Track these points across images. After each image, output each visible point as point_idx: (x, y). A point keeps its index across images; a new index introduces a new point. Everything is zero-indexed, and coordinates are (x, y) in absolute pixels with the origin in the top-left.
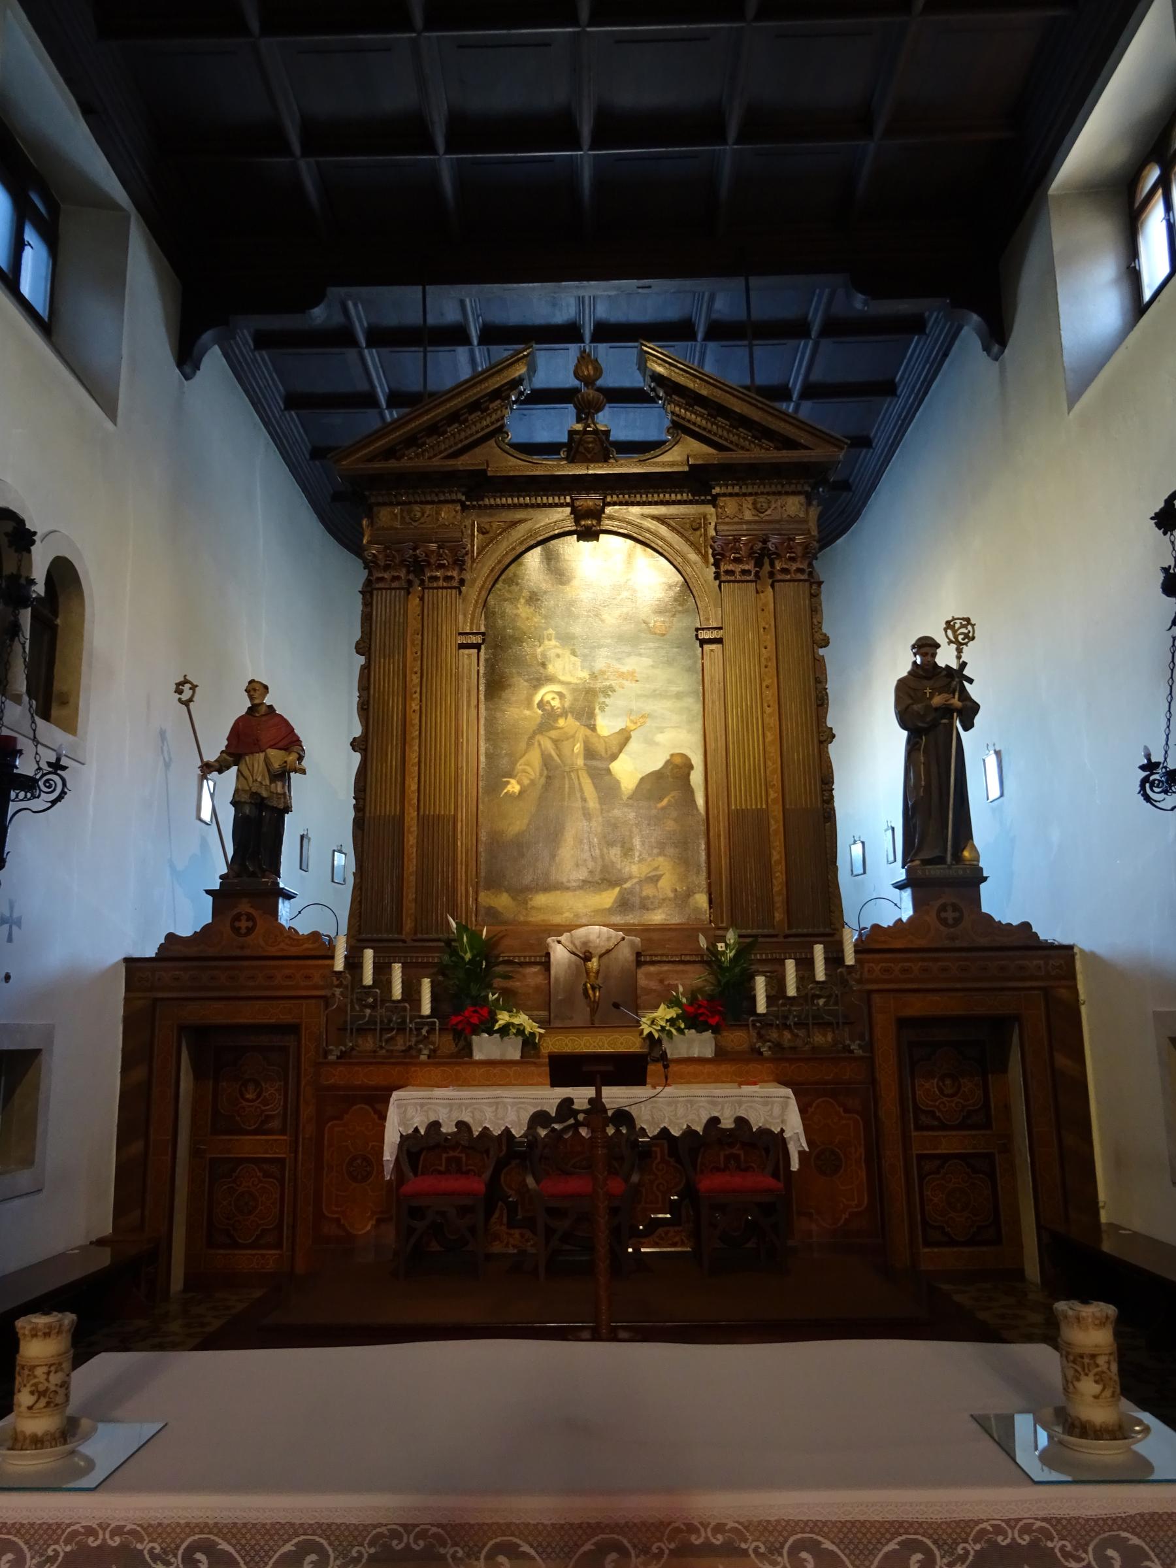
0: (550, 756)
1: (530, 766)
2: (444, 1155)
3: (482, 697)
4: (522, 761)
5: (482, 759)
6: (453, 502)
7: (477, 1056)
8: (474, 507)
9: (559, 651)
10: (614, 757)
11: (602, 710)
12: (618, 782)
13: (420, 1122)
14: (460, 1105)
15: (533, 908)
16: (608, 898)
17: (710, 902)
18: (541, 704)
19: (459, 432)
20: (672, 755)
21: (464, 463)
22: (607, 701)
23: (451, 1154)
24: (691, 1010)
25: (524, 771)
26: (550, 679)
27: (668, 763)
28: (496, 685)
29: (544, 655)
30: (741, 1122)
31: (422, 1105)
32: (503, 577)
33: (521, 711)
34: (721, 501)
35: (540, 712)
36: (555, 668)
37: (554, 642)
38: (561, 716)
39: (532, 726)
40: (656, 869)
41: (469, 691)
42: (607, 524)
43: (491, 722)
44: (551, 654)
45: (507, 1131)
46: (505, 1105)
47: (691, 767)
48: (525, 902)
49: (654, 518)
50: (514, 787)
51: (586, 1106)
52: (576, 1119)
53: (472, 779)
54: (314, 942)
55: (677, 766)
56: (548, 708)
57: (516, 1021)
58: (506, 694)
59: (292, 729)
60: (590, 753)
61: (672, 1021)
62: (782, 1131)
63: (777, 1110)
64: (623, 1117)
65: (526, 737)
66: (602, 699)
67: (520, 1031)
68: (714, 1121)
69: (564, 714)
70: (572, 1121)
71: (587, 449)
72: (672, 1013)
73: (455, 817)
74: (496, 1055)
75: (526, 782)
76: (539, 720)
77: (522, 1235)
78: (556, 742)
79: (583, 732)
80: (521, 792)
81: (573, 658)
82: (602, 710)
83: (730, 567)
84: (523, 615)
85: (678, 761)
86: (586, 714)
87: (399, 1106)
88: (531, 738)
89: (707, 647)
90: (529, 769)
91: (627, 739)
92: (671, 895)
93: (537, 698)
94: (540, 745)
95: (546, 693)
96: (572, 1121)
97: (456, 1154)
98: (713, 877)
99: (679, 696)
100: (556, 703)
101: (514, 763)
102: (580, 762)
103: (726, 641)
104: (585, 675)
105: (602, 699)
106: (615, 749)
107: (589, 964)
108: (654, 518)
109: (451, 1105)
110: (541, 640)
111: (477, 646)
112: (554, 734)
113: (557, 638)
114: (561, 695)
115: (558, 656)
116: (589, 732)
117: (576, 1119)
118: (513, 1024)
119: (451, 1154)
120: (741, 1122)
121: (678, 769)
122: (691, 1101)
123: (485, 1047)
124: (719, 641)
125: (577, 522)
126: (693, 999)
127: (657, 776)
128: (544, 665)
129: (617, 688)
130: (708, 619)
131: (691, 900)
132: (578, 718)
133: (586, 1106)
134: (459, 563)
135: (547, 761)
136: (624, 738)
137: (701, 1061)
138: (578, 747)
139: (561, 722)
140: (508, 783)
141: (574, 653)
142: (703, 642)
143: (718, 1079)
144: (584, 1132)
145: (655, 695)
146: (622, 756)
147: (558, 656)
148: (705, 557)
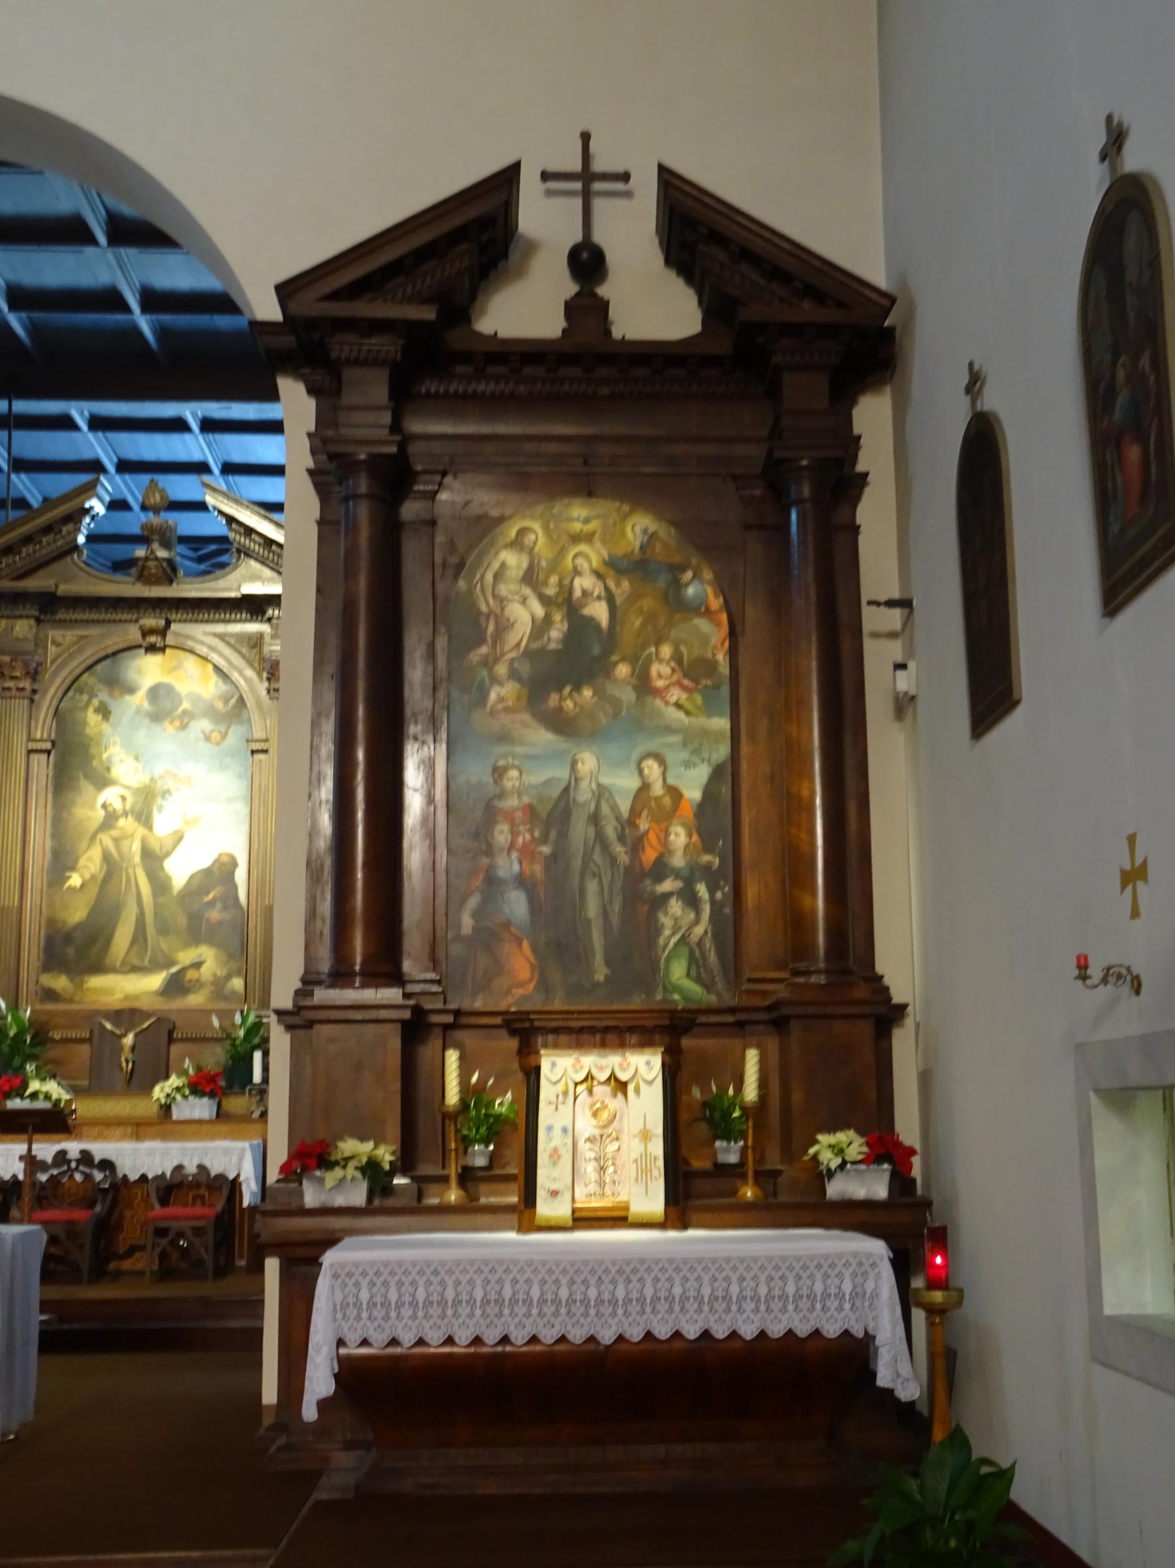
0: (111, 854)
1: (90, 863)
4: (86, 856)
6: (27, 617)
8: (49, 621)
10: (168, 854)
15: (88, 989)
16: (156, 981)
18: (104, 806)
19: (34, 552)
21: (34, 584)
25: (86, 867)
29: (109, 759)
30: (202, 1168)
32: (75, 685)
33: (92, 806)
36: (116, 772)
38: (122, 816)
40: (200, 956)
42: (170, 639)
48: (81, 984)
49: (216, 635)
50: (75, 880)
59: (321, 523)
61: (178, 1089)
62: (238, 1176)
63: (235, 1159)
64: (107, 1165)
65: (89, 836)
68: (179, 1168)
69: (125, 814)
75: (87, 876)
78: (116, 841)
79: (141, 831)
80: (82, 886)
81: (135, 763)
82: (160, 809)
85: (225, 859)
86: (144, 817)
91: (180, 839)
94: (101, 841)
95: (110, 796)
96: (65, 1168)
100: (118, 805)
101: (76, 861)
102: (137, 859)
103: (271, 751)
104: (144, 779)
105: (159, 801)
108: (216, 635)
111: (49, 752)
112: (114, 833)
114: (124, 798)
115: (122, 761)
120: (202, 1168)
121: (223, 871)
122: (151, 1152)
124: (265, 751)
127: (207, 872)
134: (34, 675)
135: (106, 857)
136: (179, 838)
137: (200, 1122)
138: (136, 847)
139: (122, 822)
140: (69, 877)
141: (137, 758)
143: (213, 1137)
148: (259, 674)
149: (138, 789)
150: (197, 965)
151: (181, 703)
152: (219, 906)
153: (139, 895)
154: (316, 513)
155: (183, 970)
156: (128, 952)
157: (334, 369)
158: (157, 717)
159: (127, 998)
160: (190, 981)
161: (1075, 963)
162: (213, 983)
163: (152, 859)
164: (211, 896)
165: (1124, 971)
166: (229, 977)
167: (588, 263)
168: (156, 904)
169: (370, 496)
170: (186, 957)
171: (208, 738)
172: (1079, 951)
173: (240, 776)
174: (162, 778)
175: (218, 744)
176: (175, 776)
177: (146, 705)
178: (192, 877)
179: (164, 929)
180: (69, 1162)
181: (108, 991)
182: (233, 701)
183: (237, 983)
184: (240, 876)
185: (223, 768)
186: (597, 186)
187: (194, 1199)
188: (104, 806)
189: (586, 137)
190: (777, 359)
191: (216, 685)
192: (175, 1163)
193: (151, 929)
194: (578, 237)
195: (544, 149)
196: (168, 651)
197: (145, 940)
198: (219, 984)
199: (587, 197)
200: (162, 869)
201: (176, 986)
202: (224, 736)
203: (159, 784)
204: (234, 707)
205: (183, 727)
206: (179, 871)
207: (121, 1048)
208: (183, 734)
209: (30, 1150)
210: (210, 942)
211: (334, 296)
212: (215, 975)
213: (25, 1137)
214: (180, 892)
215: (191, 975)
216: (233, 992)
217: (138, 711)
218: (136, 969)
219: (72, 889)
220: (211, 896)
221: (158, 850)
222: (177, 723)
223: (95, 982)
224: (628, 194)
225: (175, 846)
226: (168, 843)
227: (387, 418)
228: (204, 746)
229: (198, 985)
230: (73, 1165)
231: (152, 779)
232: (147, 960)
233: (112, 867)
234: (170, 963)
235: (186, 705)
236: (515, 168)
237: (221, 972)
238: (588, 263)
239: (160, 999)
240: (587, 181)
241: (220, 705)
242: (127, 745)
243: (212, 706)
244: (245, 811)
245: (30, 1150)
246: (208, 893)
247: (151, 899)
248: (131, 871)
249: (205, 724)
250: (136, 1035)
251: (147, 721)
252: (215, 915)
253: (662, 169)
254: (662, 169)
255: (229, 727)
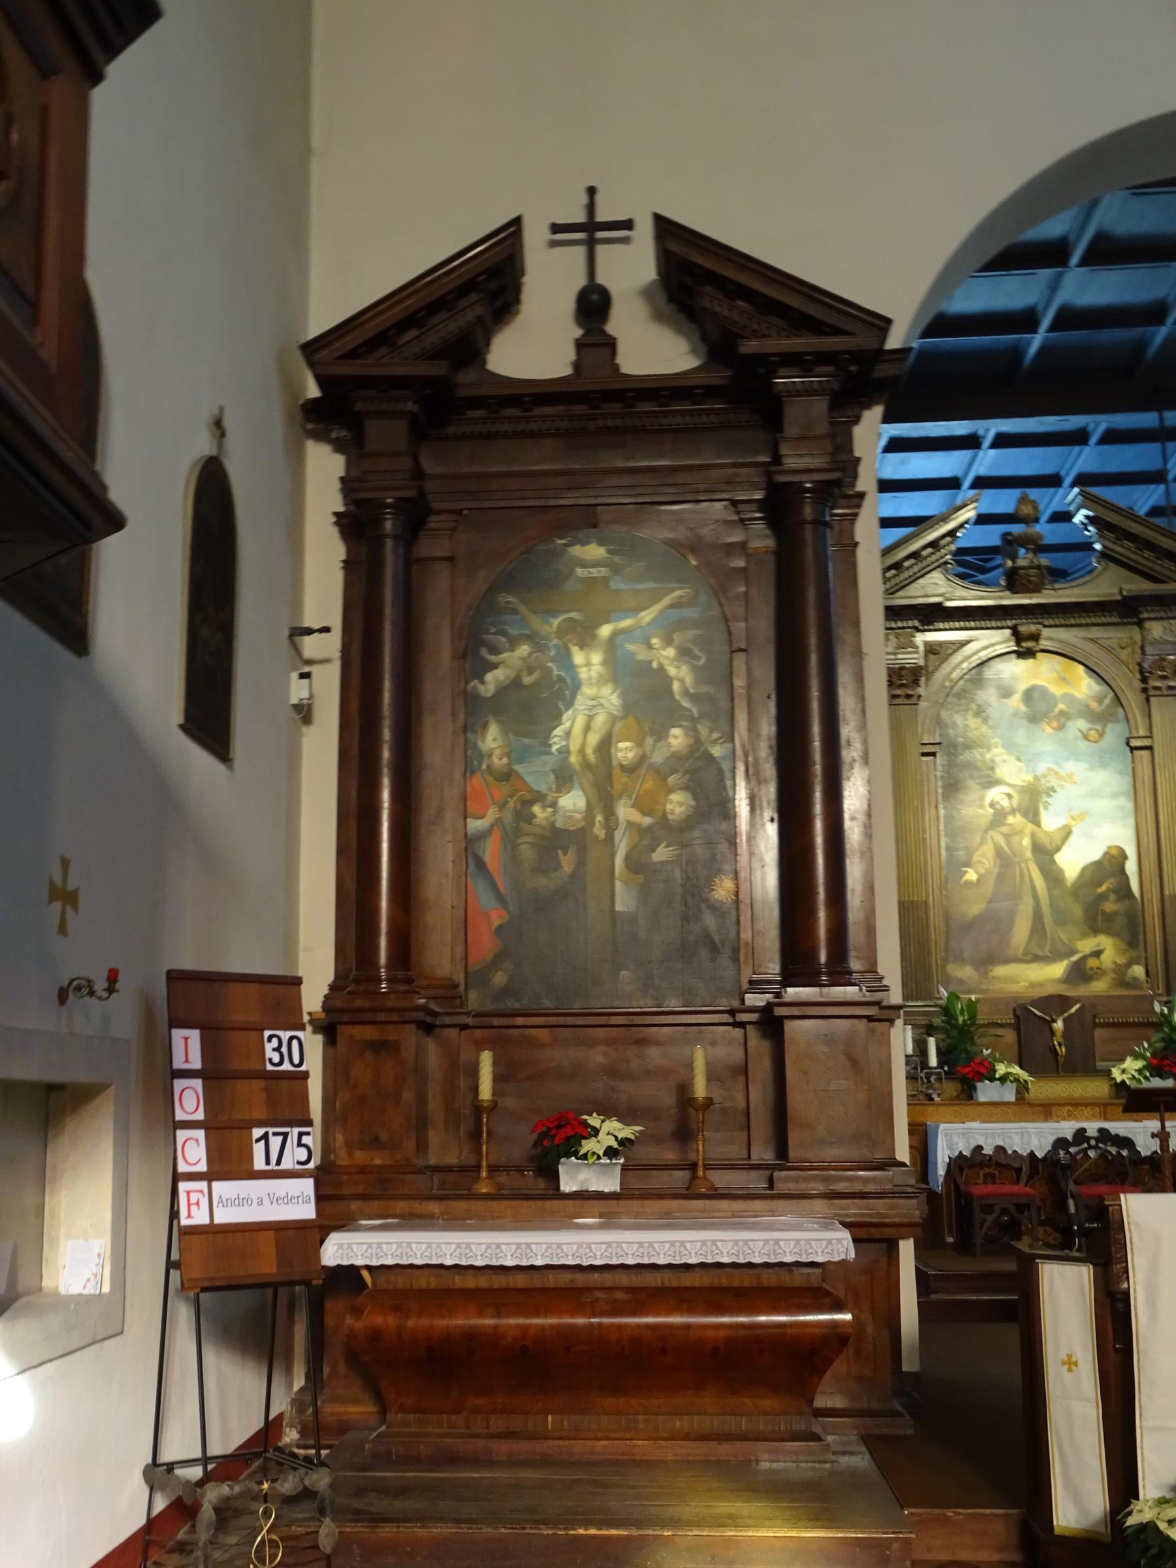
2: (981, 1172)
3: (940, 797)
4: (977, 853)
5: (943, 852)
7: (982, 1098)
9: (1005, 757)
10: (1058, 849)
11: (1046, 808)
12: (1061, 871)
13: (964, 1147)
14: (993, 1134)
16: (1058, 970)
17: (1147, 973)
18: (992, 805)
20: (1109, 848)
22: (1050, 800)
23: (987, 1170)
24: (1155, 1062)
25: (980, 862)
26: (997, 782)
27: (1106, 854)
28: (953, 787)
29: (992, 760)
31: (964, 1134)
34: (1148, 624)
35: (991, 811)
36: (1002, 772)
37: (999, 750)
38: (1009, 814)
39: (985, 822)
40: (1099, 945)
41: (25, 398)
42: (1044, 643)
43: (949, 818)
44: (998, 760)
45: (1032, 1154)
46: (1028, 1133)
47: (1125, 857)
48: (987, 973)
50: (971, 875)
51: (1096, 1134)
52: (1089, 1143)
53: (936, 869)
54: (776, 997)
55: (1113, 857)
56: (998, 807)
57: (1013, 1071)
58: (960, 796)
60: (1037, 848)
61: (1140, 1071)
66: (1045, 798)
67: (1017, 1080)
69: (1013, 811)
70: (1086, 1145)
71: (1030, 582)
72: (1140, 1064)
73: (926, 902)
74: (996, 1098)
76: (991, 817)
77: (1045, 1231)
78: (1007, 837)
79: (1030, 827)
80: (978, 880)
82: (1046, 808)
83: (1158, 684)
84: (973, 726)
85: (1115, 852)
86: (1032, 815)
87: (946, 1135)
88: (986, 831)
89: (1136, 752)
90: (985, 861)
92: (1113, 966)
93: (988, 800)
95: (995, 794)
96: (1086, 1145)
97: (991, 1171)
98: (1149, 951)
99: (1114, 795)
100: (1005, 803)
102: (1029, 854)
104: (1029, 778)
105: (1045, 798)
106: (1059, 843)
107: (1055, 1025)
109: (987, 1134)
110: (989, 749)
112: (1004, 829)
113: (1003, 747)
114: (1009, 796)
115: (1005, 761)
116: (1034, 828)
117: (1089, 1143)
118: (1010, 1074)
119: (987, 1170)
121: (1113, 862)
123: (986, 1092)
125: (1018, 643)
126: (1154, 1055)
127: (1098, 865)
128: (992, 769)
129: (1058, 789)
130: (1137, 729)
131: (1130, 971)
132: (1025, 815)
133: (1096, 1134)
135: (999, 852)
136: (1067, 833)
137: (1008, 1104)
138: (1026, 842)
139: (1011, 820)
140: (966, 872)
141: (1018, 759)
142: (1132, 749)
144: (1092, 1153)
145: (1095, 794)
146: (1064, 848)
147: (1005, 761)
149: (1023, 787)
150: (1097, 954)
151: (1056, 705)
152: (1112, 897)
153: (1033, 887)
154: (342, 555)
155: (1084, 959)
156: (1028, 943)
157: (356, 424)
158: (1034, 719)
159: (1033, 985)
160: (1091, 969)
161: (106, 975)
162: (1114, 971)
163: (1045, 853)
164: (1104, 888)
165: (84, 983)
166: (1129, 965)
167: (593, 305)
168: (1051, 896)
169: (395, 537)
170: (1086, 946)
171: (1086, 737)
172: (112, 966)
173: (1121, 773)
174: (1045, 776)
175: (1096, 742)
176: (1057, 773)
177: (1023, 708)
178: (1084, 869)
179: (1061, 920)
180: (1088, 1139)
181: (1013, 980)
182: (1107, 701)
183: (1138, 971)
184: (1131, 867)
185: (1104, 765)
186: (600, 235)
187: (985, 1175)
188: (992, 805)
189: (592, 191)
190: (359, 407)
191: (1089, 687)
192: (973, 1144)
193: (1048, 920)
194: (581, 281)
195: (545, 205)
196: (1039, 655)
197: (1044, 931)
198: (1120, 972)
199: (591, 244)
200: (1054, 862)
201: (1080, 973)
202: (1101, 735)
203: (1043, 781)
204: (1109, 706)
205: (1061, 727)
206: (1073, 861)
207: (1052, 1033)
208: (1061, 734)
209: (1163, 1127)
210: (1109, 932)
211: (352, 355)
212: (1115, 963)
213: (1158, 1115)
214: (1074, 884)
215: (1092, 963)
216: (1136, 979)
217: (1015, 714)
218: (1037, 959)
219: (969, 884)
220: (1104, 888)
221: (1048, 846)
222: (1055, 724)
223: (1000, 971)
224: (626, 241)
225: (1064, 839)
226: (1057, 840)
227: (406, 463)
228: (1083, 744)
229: (1099, 973)
230: (1093, 1142)
231: (1036, 778)
232: (1047, 949)
233: (1005, 860)
234: (1074, 952)
235: (1061, 706)
236: (513, 229)
237: (1121, 960)
238: (593, 305)
239: (1065, 986)
240: (591, 231)
241: (1094, 705)
242: (1009, 746)
243: (1087, 706)
244: (1130, 805)
245: (1163, 1127)
246: (1100, 885)
247: (1045, 890)
248: (1023, 865)
249: (1082, 724)
250: (1065, 1021)
251: (1025, 722)
252: (1110, 906)
253: (517, 221)
254: (517, 221)
255: (1105, 726)
